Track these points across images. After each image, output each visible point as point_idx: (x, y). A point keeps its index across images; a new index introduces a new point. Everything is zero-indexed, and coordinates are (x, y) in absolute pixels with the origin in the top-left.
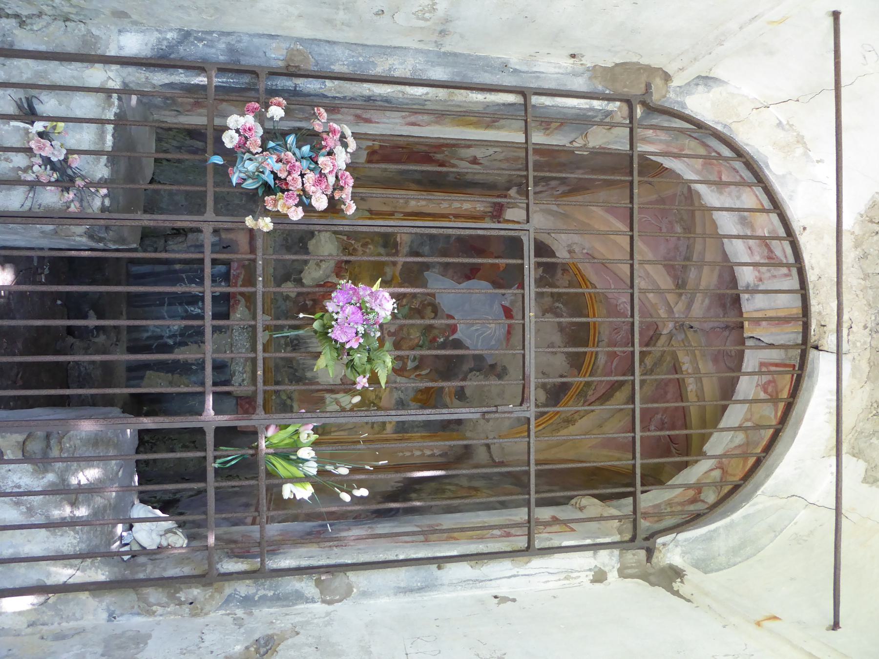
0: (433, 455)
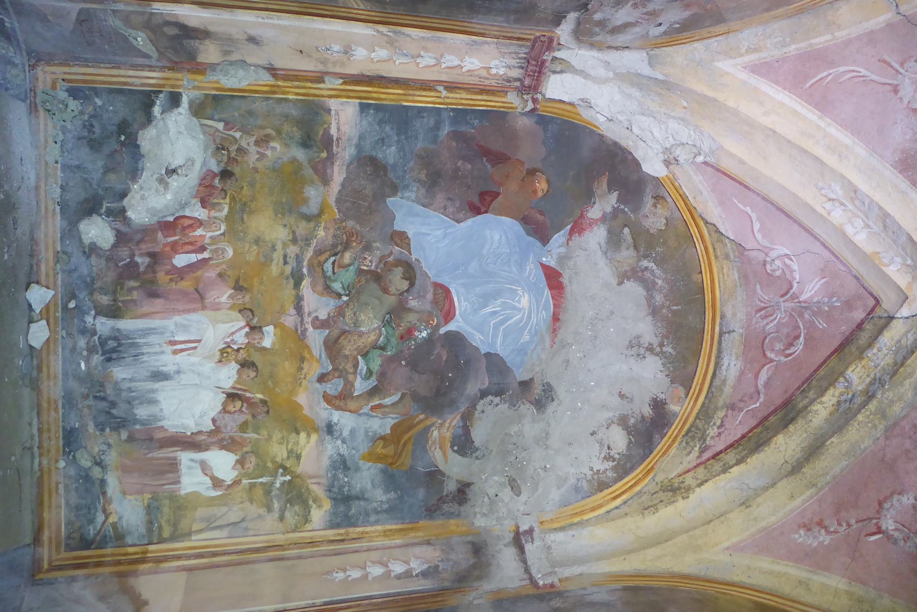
0: (408, 574)
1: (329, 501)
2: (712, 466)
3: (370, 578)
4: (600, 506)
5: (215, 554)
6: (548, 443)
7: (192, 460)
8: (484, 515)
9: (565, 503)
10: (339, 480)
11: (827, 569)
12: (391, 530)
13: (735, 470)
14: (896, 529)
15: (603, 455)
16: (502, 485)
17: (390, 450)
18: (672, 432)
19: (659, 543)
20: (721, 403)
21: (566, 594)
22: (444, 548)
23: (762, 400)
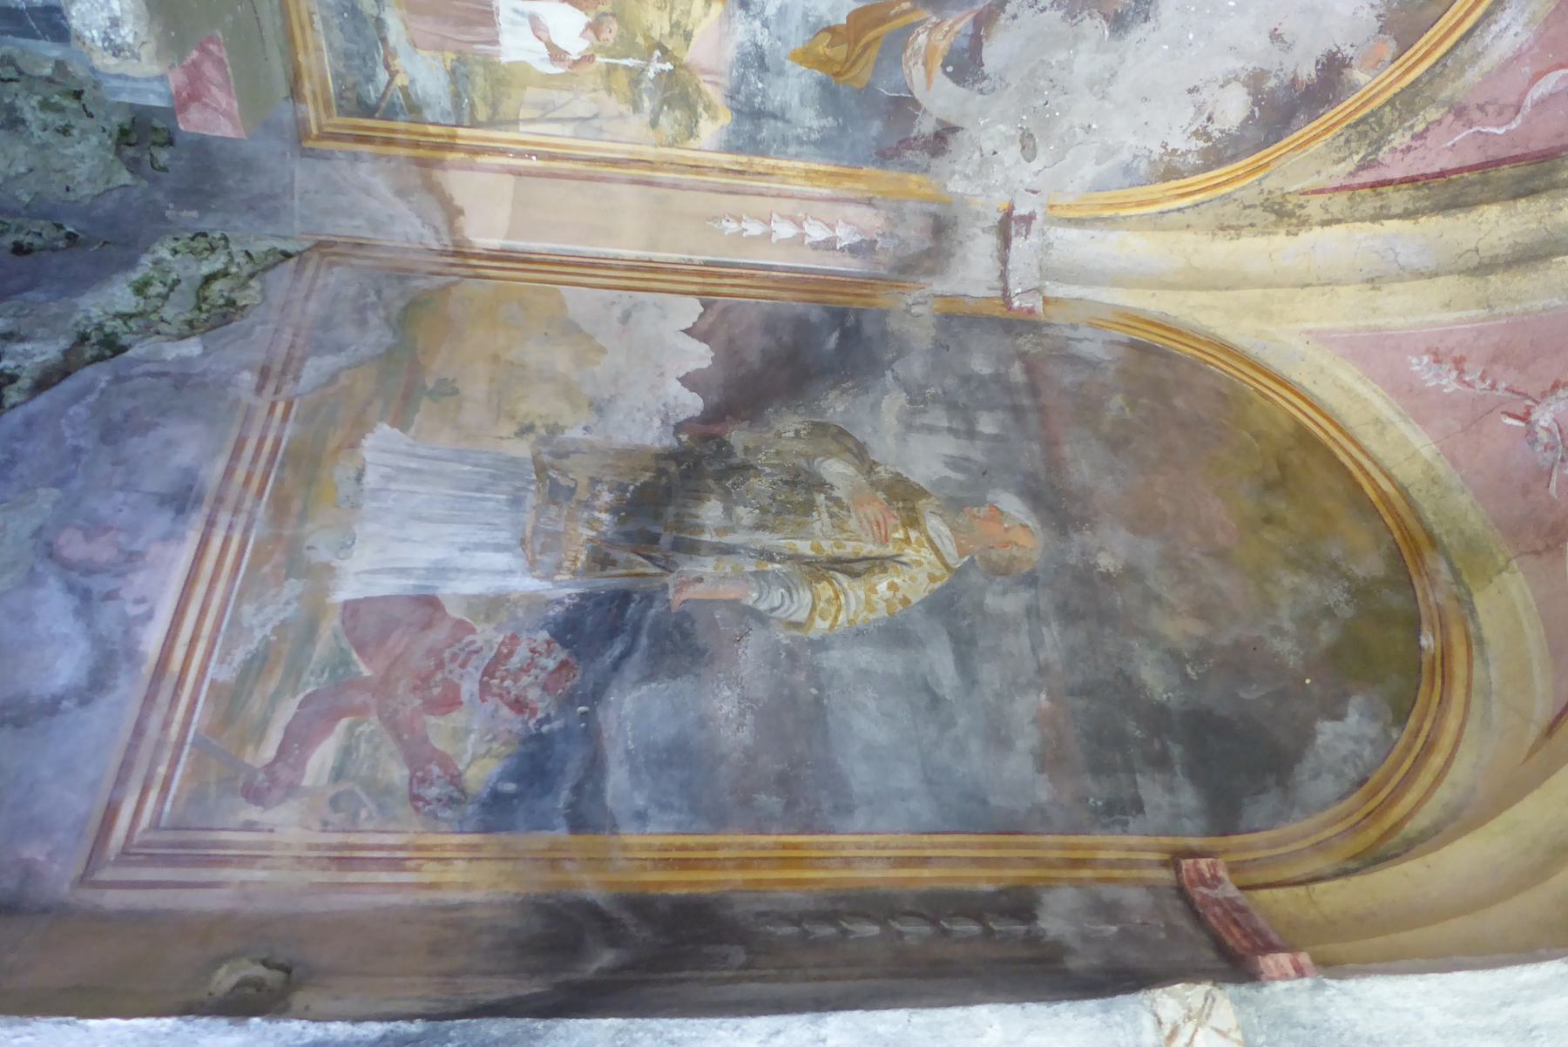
0: (829, 245)
1: (729, 112)
2: (1363, 199)
3: (774, 240)
4: (1154, 202)
5: (553, 157)
6: (1111, 89)
7: (516, 11)
8: (967, 177)
9: (1099, 186)
10: (748, 84)
11: (1422, 422)
12: (816, 172)
13: (1392, 225)
14: (1548, 430)
15: (1193, 128)
16: (1009, 140)
17: (840, 52)
18: (1330, 115)
19: (1216, 288)
20: (1445, 94)
21: (1046, 331)
22: (891, 215)
23: (1514, 126)
